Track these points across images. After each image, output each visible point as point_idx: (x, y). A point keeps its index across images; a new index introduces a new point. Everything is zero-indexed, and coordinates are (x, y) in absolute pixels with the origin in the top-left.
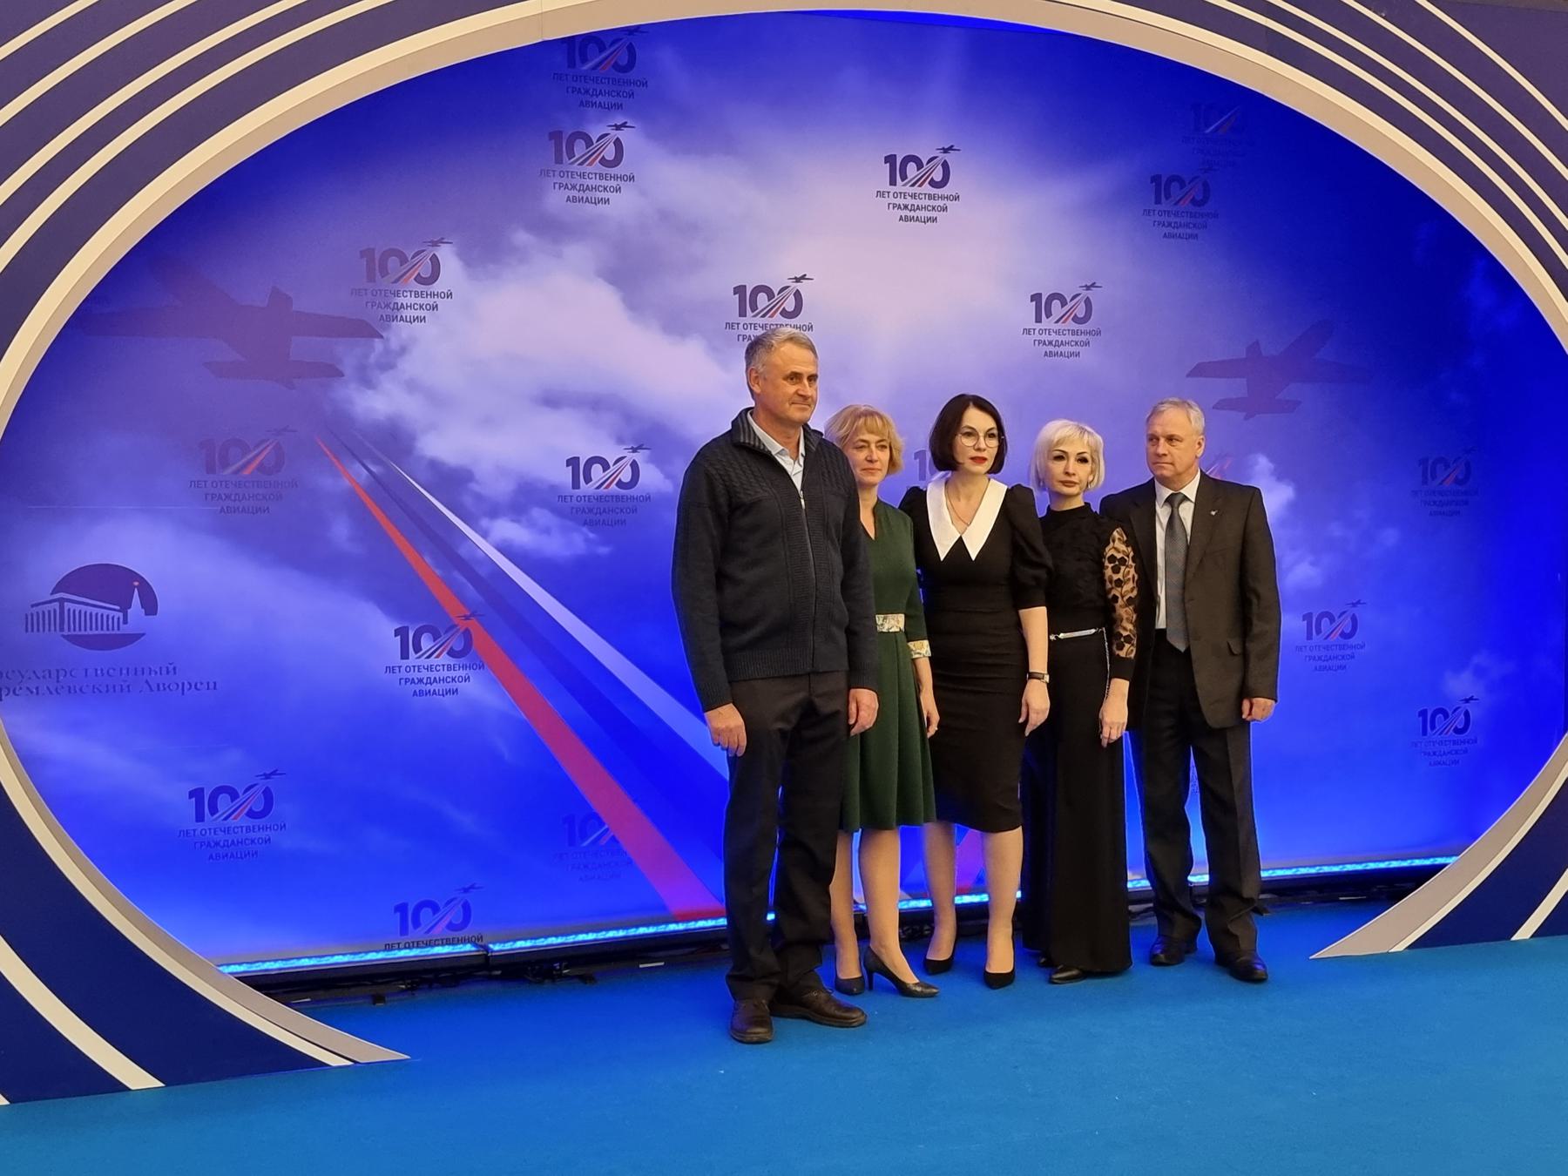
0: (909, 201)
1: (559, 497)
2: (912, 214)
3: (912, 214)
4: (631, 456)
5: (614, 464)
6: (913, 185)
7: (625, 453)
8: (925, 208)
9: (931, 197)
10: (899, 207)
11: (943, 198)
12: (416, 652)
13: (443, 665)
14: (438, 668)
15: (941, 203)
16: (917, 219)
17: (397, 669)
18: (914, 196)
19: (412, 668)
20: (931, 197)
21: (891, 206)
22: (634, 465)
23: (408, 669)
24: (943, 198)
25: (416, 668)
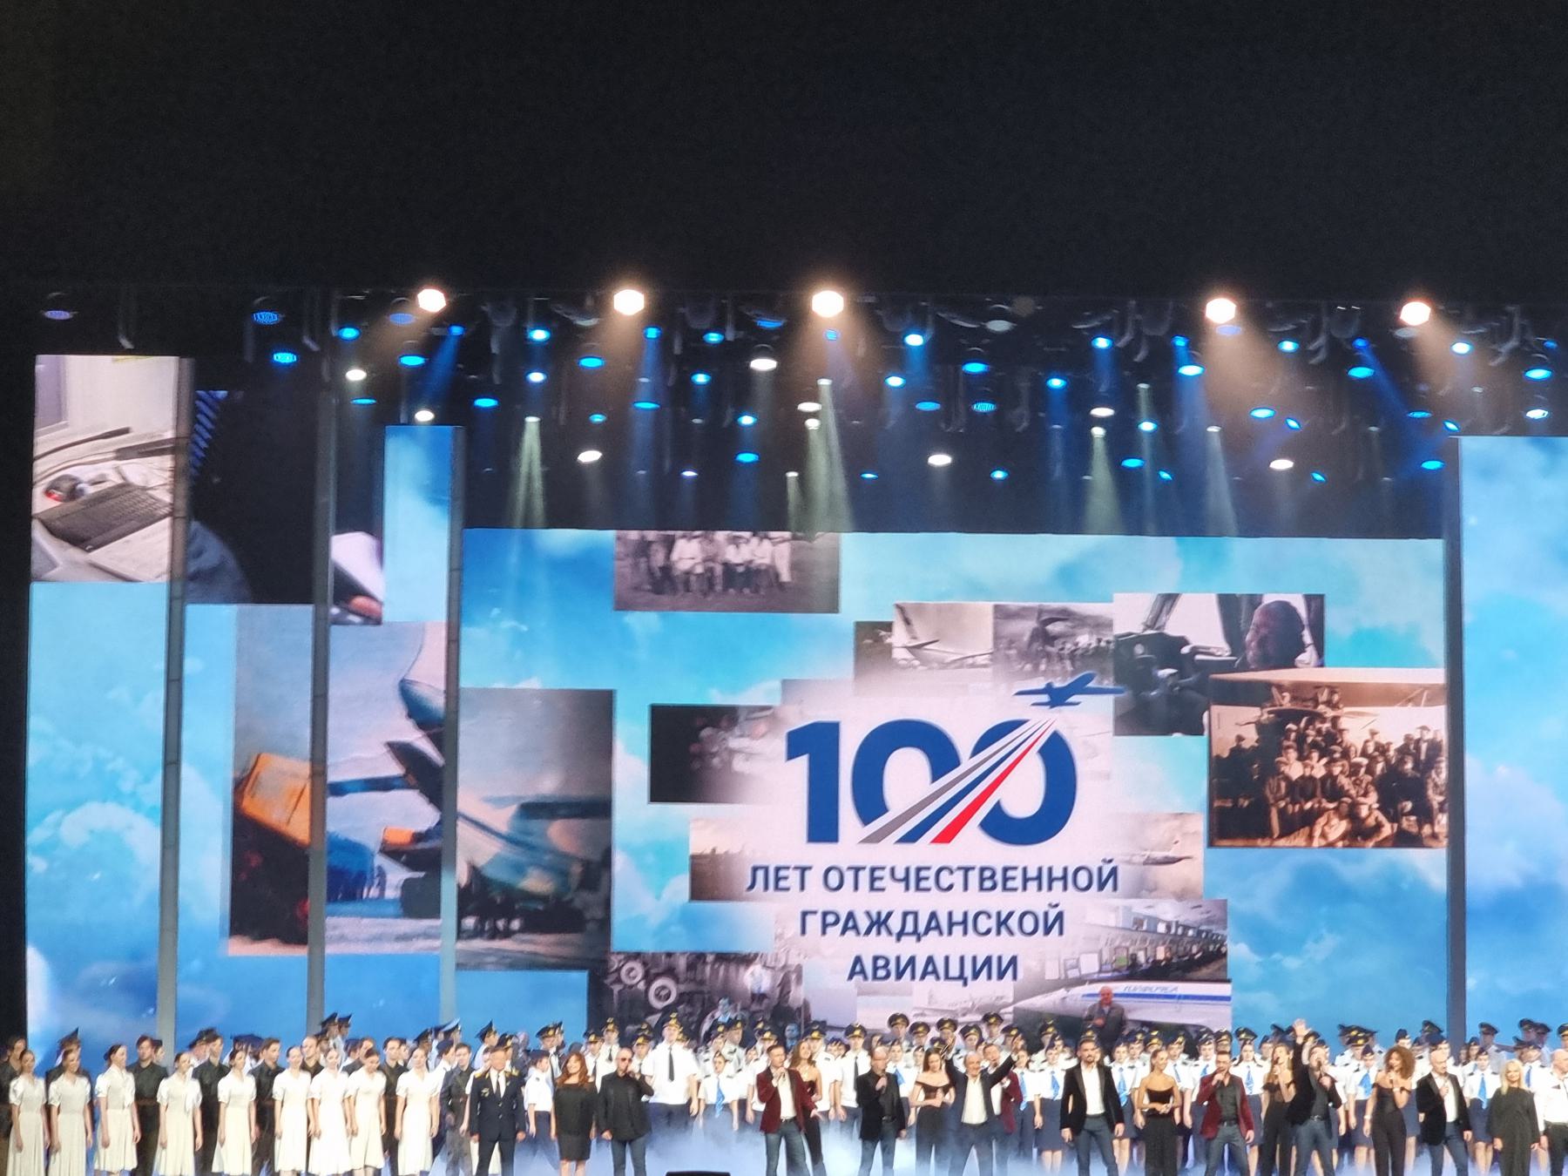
0: (895, 899)
1: (755, 869)
2: (908, 948)
3: (908, 948)
4: (1043, 721)
5: (978, 749)
6: (912, 837)
7: (1020, 708)
8: (966, 923)
9: (989, 879)
10: (850, 923)
11: (1044, 879)
12: (866, 818)
13: (967, 870)
14: (945, 879)
15: (1036, 900)
16: (930, 968)
17: (794, 877)
18: (914, 879)
19: (849, 876)
20: (989, 879)
21: (814, 923)
22: (1058, 757)
23: (834, 879)
24: (1044, 879)
25: (864, 877)
